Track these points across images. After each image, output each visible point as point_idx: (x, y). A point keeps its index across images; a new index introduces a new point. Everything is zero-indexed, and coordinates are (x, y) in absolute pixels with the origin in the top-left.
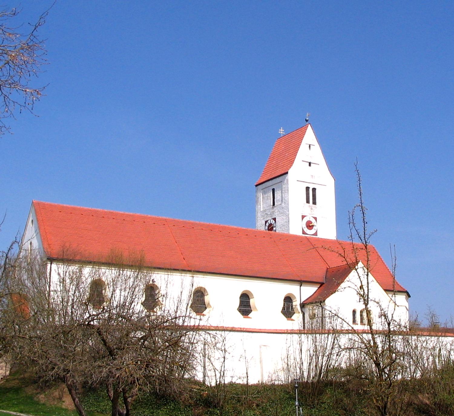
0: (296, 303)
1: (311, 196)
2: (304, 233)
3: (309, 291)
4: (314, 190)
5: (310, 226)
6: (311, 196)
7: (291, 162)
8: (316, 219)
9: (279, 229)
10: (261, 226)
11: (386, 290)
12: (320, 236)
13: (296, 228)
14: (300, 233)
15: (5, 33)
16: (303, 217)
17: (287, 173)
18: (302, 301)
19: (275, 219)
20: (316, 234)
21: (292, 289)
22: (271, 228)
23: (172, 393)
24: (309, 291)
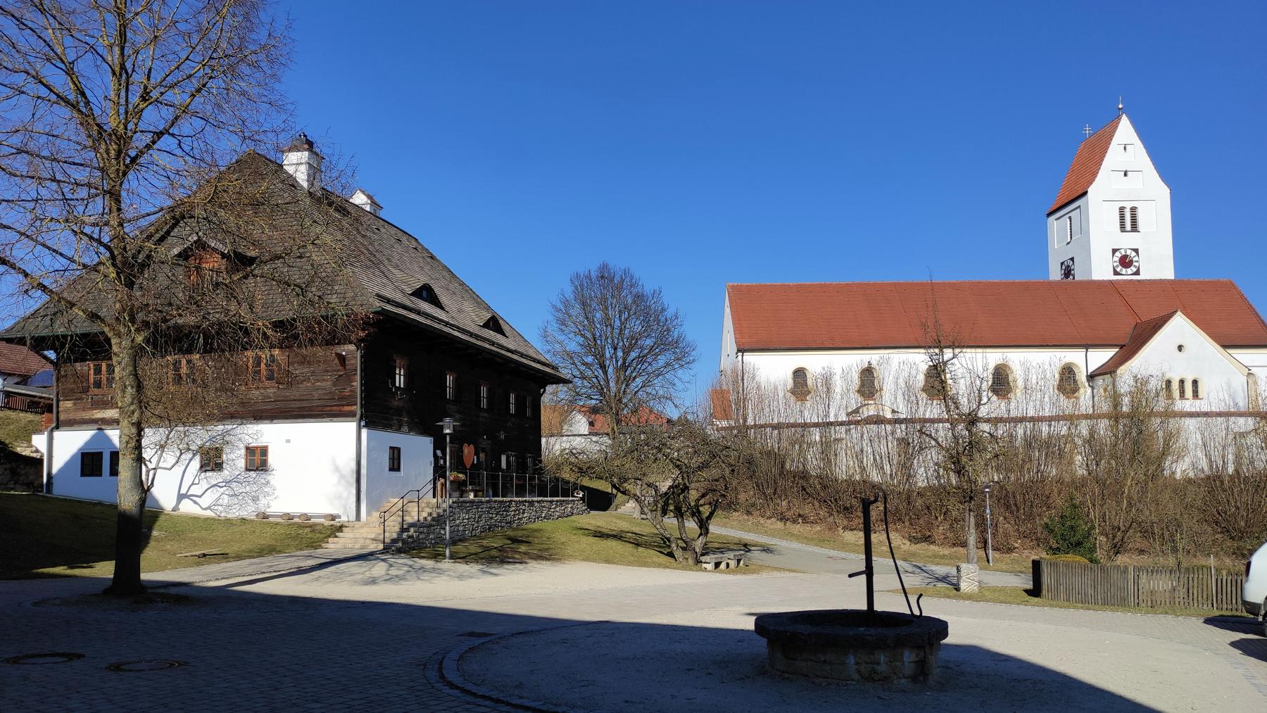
0: (1082, 377)
1: (1129, 221)
2: (1116, 273)
3: (1100, 357)
4: (1133, 210)
5: (1125, 262)
6: (1129, 221)
7: (1094, 175)
8: (1136, 251)
9: (1079, 275)
10: (1056, 274)
11: (1225, 347)
12: (1143, 276)
13: (1101, 269)
14: (1110, 276)
15: (28, 68)
16: (1114, 251)
17: (1085, 193)
18: (1090, 371)
19: (1072, 259)
20: (1137, 273)
21: (1074, 356)
22: (1068, 272)
23: (137, 353)
24: (1100, 357)
